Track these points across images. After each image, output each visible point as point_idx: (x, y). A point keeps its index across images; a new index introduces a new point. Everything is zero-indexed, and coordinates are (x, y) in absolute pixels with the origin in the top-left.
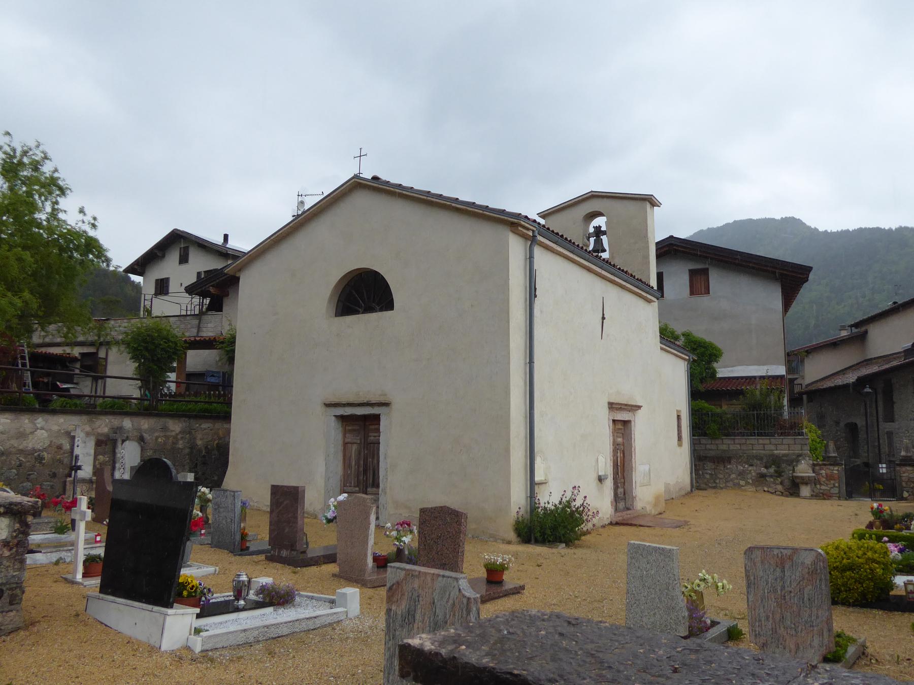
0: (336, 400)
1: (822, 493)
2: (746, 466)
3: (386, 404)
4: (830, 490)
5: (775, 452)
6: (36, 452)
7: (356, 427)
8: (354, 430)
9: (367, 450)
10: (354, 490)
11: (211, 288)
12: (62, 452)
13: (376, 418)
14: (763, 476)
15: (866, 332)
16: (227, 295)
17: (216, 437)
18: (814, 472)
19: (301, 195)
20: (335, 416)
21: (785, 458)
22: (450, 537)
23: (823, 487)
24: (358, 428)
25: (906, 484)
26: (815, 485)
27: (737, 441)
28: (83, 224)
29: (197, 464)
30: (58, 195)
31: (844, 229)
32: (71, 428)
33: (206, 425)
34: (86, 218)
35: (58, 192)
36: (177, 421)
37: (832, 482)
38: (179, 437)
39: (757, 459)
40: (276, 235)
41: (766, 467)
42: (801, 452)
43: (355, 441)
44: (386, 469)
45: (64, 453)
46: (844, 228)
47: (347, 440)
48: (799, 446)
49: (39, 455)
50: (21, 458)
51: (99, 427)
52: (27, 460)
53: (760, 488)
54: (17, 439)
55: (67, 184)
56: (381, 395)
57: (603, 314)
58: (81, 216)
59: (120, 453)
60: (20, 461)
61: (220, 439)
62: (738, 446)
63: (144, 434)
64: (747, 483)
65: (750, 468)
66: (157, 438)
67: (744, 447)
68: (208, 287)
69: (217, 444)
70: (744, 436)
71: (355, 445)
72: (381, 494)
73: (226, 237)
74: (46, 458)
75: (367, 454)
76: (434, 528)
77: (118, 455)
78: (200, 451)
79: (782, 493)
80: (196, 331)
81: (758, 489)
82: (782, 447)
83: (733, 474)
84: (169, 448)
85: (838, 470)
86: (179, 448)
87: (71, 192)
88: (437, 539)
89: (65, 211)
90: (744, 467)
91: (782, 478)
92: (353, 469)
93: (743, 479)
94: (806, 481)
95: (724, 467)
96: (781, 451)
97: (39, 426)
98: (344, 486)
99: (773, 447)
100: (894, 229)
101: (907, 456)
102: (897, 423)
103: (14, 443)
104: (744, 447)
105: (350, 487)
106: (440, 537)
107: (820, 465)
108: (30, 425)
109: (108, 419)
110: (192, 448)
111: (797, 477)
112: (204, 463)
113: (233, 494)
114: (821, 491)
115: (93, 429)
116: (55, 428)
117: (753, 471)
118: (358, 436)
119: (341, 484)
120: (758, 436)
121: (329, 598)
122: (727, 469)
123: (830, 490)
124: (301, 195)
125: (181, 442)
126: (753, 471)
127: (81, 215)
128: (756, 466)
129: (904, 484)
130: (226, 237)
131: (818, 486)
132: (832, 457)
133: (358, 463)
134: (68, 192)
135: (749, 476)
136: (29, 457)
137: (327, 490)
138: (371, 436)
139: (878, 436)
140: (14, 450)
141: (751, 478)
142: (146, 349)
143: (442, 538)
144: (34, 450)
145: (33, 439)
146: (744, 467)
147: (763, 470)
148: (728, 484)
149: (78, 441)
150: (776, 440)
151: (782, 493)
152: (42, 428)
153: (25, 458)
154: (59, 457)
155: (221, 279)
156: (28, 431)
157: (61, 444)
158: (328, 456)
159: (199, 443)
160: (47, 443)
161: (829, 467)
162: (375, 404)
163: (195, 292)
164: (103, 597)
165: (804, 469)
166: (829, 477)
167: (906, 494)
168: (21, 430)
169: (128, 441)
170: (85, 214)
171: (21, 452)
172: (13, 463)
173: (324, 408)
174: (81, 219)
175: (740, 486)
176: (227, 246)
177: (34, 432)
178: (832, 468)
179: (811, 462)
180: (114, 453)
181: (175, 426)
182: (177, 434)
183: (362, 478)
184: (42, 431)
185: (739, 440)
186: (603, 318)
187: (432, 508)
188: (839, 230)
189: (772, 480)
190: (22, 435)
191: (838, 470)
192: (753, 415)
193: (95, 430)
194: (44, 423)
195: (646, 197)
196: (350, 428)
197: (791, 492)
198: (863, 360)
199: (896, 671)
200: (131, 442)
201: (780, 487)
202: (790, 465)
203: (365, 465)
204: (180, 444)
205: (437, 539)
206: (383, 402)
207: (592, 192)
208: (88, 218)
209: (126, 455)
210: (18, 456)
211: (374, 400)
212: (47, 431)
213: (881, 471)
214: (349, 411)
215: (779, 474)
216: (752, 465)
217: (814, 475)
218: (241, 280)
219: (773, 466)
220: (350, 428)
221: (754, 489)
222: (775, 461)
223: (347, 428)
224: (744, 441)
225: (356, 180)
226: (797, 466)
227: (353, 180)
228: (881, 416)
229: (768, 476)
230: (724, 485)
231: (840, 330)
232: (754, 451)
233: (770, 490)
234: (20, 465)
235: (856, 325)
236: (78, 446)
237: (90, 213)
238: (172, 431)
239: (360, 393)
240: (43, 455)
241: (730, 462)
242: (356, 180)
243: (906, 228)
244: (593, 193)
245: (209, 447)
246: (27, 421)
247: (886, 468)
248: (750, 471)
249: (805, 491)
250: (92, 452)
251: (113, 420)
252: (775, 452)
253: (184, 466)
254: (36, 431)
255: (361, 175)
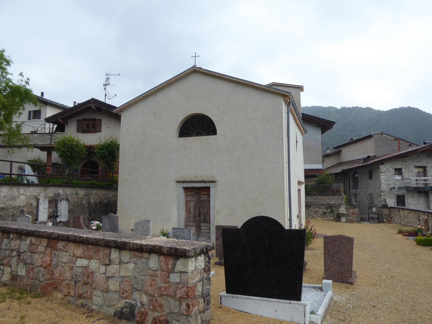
0: (184, 180)
1: (350, 220)
2: (318, 209)
3: (214, 182)
4: (353, 219)
5: (330, 202)
6: (21, 208)
7: (193, 193)
8: (192, 195)
9: (200, 204)
10: (193, 225)
11: (60, 119)
12: (33, 207)
13: (208, 189)
14: (325, 213)
15: (341, 151)
16: (67, 124)
17: (99, 197)
18: (347, 211)
19: (108, 75)
20: (183, 187)
21: (334, 205)
22: (346, 250)
23: (350, 218)
24: (194, 193)
25: (385, 216)
26: (347, 216)
27: (313, 198)
28: (22, 82)
29: (91, 212)
30: (5, 65)
31: (307, 106)
32: (36, 194)
33: (94, 191)
34: (23, 79)
35: (5, 63)
36: (82, 190)
37: (354, 215)
38: (83, 198)
39: (322, 206)
40: (146, 94)
41: (326, 209)
42: (341, 202)
43: (193, 200)
44: (214, 214)
45: (34, 208)
46: (307, 106)
47: (188, 200)
48: (340, 200)
49: (22, 209)
50: (14, 211)
51: (49, 194)
52: (17, 212)
53: (323, 218)
54: (11, 201)
55: (11, 59)
56: (210, 177)
57: (297, 140)
58: (21, 77)
59: (59, 207)
60: (13, 213)
61: (100, 198)
62: (314, 200)
63: (69, 197)
64: (318, 216)
65: (319, 210)
66: (74, 198)
67: (317, 201)
68: (58, 119)
69: (100, 201)
70: (316, 195)
71: (193, 202)
72: (212, 226)
73: (42, 94)
74: (25, 211)
75: (200, 206)
76: (334, 246)
77: (59, 208)
78: (92, 205)
79: (333, 220)
80: (50, 142)
81: (322, 219)
82: (333, 200)
83: (312, 212)
84: (79, 204)
85: (357, 210)
86: (83, 204)
87: (13, 63)
88: (337, 252)
89: (12, 74)
90: (317, 209)
91: (333, 214)
92: (192, 214)
93: (316, 214)
94: (343, 215)
95: (308, 209)
96: (332, 202)
97: (21, 193)
98: (187, 223)
99: (329, 200)
100: (326, 107)
101: (385, 204)
102: (359, 190)
103: (10, 202)
104: (317, 201)
105: (190, 223)
106: (339, 251)
107: (349, 208)
108: (17, 193)
109: (53, 189)
110: (89, 204)
111: (340, 213)
112: (94, 212)
113: (189, 230)
114: (350, 219)
115: (46, 195)
116: (29, 194)
117: (321, 211)
118: (195, 197)
119: (185, 222)
120: (322, 195)
121: (312, 286)
122: (309, 210)
123: (353, 219)
124: (108, 75)
125: (84, 201)
126: (321, 211)
127: (21, 77)
128: (322, 209)
129: (384, 216)
130: (42, 94)
131: (348, 217)
132: (354, 205)
133: (195, 211)
134: (11, 63)
135: (319, 213)
136: (18, 210)
137: (179, 224)
138: (202, 198)
139: (350, 194)
140: (10, 207)
141: (320, 214)
142: (68, 151)
143: (340, 251)
144: (20, 207)
145: (18, 200)
146: (317, 209)
147: (325, 210)
148: (310, 217)
149: (41, 201)
150: (331, 197)
151: (333, 220)
152: (23, 195)
153: (16, 211)
154: (31, 210)
155: (64, 116)
156: (17, 196)
157: (32, 203)
158: (179, 207)
159: (92, 201)
160: (26, 202)
161: (353, 209)
162: (207, 181)
163: (51, 121)
164: (235, 296)
165: (342, 210)
166: (353, 213)
167: (385, 220)
168: (13, 195)
169: (63, 201)
170: (23, 76)
171: (14, 208)
172: (10, 214)
173: (176, 183)
174: (21, 79)
175: (315, 218)
176: (43, 98)
177: (19, 197)
178: (354, 209)
179: (345, 207)
180: (56, 207)
181: (82, 192)
182: (83, 197)
183: (197, 218)
184: (22, 196)
185: (314, 197)
186: (297, 142)
187: (332, 236)
188: (305, 106)
189: (329, 215)
190: (14, 199)
191: (357, 210)
192: (321, 186)
193: (47, 195)
194: (23, 191)
195: (300, 87)
196: (190, 193)
197: (337, 219)
198: (339, 162)
199: (208, 283)
200: (64, 201)
201: (332, 218)
202: (336, 208)
203: (199, 212)
204: (84, 202)
205: (337, 252)
206: (213, 181)
207: (274, 83)
208: (25, 79)
209: (62, 208)
210: (12, 210)
211: (206, 179)
212: (25, 196)
213: (373, 211)
214: (191, 185)
215: (332, 212)
216: (320, 208)
217: (347, 212)
218: (122, 117)
219: (329, 209)
220: (190, 193)
221: (321, 219)
222: (330, 206)
223: (188, 193)
224: (316, 198)
225: (194, 68)
226: (340, 208)
227: (193, 69)
228: (352, 187)
229: (327, 213)
230: (308, 217)
231: (327, 149)
232: (321, 202)
233: (328, 219)
234: (13, 215)
235: (336, 148)
236: (41, 204)
237: (26, 75)
238: (80, 195)
239: (198, 176)
240: (24, 209)
241: (311, 207)
242: (194, 68)
243: (331, 107)
244: (274, 83)
245: (96, 203)
246: (15, 191)
247: (376, 209)
248: (319, 211)
249: (343, 219)
250: (47, 207)
251: (55, 189)
252: (330, 202)
253: (86, 213)
254: (20, 196)
255: (196, 66)
